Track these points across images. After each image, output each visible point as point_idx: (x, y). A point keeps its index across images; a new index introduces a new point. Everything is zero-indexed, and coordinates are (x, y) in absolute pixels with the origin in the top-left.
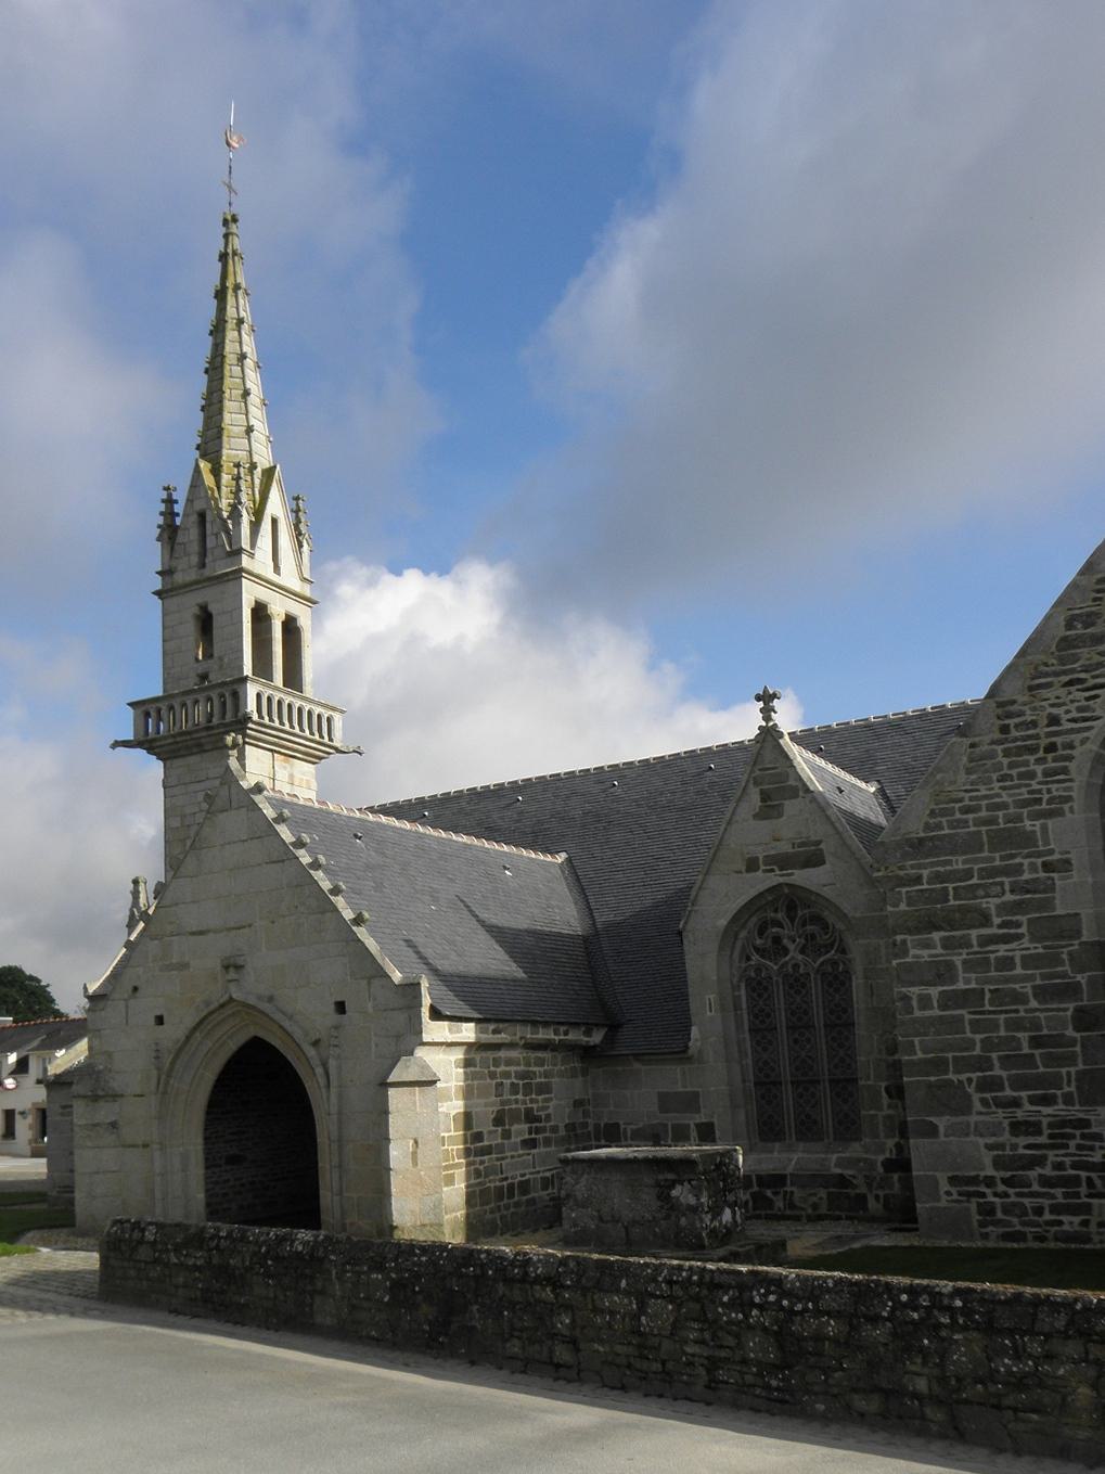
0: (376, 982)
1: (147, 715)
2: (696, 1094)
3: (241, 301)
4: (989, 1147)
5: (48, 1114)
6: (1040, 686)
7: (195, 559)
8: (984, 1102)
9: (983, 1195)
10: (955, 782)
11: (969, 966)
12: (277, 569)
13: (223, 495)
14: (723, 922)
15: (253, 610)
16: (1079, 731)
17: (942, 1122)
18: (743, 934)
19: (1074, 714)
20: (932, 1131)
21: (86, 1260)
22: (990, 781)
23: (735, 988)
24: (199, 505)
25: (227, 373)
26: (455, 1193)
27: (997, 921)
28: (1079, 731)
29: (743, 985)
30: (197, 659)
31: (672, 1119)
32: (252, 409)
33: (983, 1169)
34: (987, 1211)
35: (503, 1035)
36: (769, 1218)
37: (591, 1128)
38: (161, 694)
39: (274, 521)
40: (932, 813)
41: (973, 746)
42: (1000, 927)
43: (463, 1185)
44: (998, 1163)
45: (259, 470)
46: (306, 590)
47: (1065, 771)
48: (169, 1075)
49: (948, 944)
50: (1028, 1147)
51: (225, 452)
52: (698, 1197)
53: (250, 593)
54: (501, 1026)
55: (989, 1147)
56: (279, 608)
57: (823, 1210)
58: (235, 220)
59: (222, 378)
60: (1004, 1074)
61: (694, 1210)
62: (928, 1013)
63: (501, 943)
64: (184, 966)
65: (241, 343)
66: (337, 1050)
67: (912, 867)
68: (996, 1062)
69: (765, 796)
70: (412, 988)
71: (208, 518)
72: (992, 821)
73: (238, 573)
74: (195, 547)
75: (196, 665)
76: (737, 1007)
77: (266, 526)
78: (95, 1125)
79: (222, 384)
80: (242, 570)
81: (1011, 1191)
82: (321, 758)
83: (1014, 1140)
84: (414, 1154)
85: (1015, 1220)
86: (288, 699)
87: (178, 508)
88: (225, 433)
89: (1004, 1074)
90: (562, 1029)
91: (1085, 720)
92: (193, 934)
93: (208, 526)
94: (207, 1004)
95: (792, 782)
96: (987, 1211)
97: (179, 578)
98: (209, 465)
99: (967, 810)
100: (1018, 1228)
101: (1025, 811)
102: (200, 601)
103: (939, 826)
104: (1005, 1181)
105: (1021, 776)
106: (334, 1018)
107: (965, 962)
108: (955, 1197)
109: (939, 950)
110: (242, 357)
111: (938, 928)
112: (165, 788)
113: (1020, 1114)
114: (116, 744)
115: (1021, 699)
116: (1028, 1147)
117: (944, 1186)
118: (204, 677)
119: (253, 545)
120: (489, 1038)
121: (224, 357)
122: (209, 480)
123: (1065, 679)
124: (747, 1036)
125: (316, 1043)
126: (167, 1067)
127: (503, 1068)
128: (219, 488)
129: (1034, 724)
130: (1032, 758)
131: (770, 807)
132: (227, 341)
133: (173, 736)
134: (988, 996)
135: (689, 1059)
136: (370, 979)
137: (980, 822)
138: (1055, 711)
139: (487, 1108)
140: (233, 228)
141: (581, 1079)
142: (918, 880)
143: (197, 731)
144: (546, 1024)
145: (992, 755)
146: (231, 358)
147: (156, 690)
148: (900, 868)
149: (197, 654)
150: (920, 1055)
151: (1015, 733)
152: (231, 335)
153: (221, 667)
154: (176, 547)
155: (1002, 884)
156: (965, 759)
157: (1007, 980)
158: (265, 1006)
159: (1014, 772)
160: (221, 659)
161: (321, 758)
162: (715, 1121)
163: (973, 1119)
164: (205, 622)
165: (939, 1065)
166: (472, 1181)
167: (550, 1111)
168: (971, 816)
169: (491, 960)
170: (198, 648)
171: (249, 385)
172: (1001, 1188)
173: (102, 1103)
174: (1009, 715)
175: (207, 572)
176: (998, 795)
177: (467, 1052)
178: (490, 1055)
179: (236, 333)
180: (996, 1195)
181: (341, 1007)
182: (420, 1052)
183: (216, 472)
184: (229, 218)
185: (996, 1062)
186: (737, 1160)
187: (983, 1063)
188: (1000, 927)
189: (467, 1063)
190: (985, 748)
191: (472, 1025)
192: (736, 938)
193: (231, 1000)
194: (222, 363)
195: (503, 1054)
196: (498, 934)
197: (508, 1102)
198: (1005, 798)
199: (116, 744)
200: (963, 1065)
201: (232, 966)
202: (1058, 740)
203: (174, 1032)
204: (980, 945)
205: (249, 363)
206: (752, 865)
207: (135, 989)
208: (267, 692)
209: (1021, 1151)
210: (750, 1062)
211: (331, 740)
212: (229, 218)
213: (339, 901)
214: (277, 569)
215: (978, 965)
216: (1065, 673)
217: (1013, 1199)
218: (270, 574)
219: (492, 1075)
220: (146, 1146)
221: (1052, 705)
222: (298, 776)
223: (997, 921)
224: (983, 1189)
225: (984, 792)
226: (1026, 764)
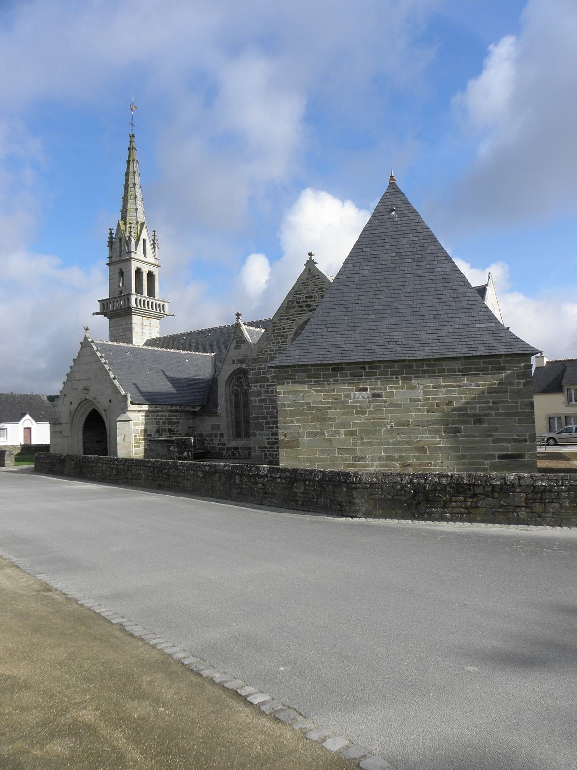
0: (119, 394)
1: (104, 304)
2: (219, 425)
3: (135, 164)
4: (267, 439)
5: (26, 427)
6: (281, 319)
7: (118, 253)
8: (266, 427)
9: (265, 451)
10: (263, 344)
11: (265, 392)
12: (145, 256)
13: (127, 232)
14: (226, 378)
15: (136, 271)
16: (289, 331)
17: (258, 432)
18: (233, 381)
19: (288, 327)
20: (255, 435)
21: (32, 466)
22: (270, 344)
23: (230, 396)
24: (119, 236)
25: (129, 190)
26: (142, 448)
27: (271, 381)
28: (289, 331)
29: (233, 395)
30: (119, 286)
31: (215, 432)
32: (138, 202)
33: (265, 444)
34: (266, 455)
35: (159, 408)
36: (235, 459)
37: (196, 434)
38: (108, 297)
39: (144, 240)
40: (258, 352)
41: (267, 334)
42: (271, 382)
43: (143, 448)
44: (269, 443)
45: (140, 223)
46: (157, 262)
47: (286, 342)
48: (73, 418)
49: (261, 387)
50: (275, 439)
51: (128, 217)
52: (174, 449)
53: (134, 265)
54: (158, 406)
55: (267, 439)
56: (145, 270)
57: (247, 457)
58: (133, 136)
59: (128, 192)
60: (271, 420)
61: (174, 452)
62: (256, 404)
63: (171, 382)
64: (76, 389)
65: (134, 179)
66: (110, 412)
67: (254, 366)
68: (269, 417)
69: (237, 343)
70: (126, 396)
71: (122, 240)
72: (270, 354)
73: (130, 259)
74: (118, 250)
75: (118, 288)
76: (231, 401)
77: (141, 242)
78: (56, 432)
79: (128, 194)
80: (131, 258)
81: (271, 450)
82: (161, 318)
83: (272, 437)
84: (124, 439)
85: (271, 458)
86: (151, 301)
87: (114, 236)
88: (128, 211)
89: (271, 420)
90: (182, 407)
91: (290, 329)
92: (78, 380)
93: (122, 242)
94: (81, 399)
95: (243, 339)
96: (266, 455)
97: (114, 259)
98: (123, 222)
99: (266, 351)
100: (272, 459)
101: (277, 352)
102: (120, 267)
103: (259, 355)
104: (269, 448)
105: (277, 343)
106: (109, 404)
107: (264, 391)
108: (260, 452)
109: (259, 388)
110: (135, 184)
111: (259, 382)
112: (110, 327)
113: (273, 431)
114: (94, 314)
115: (278, 322)
116: (275, 439)
117: (257, 449)
118: (121, 292)
119: (136, 249)
120: (151, 409)
121: (128, 185)
122: (122, 227)
123: (287, 317)
124: (234, 409)
125: (105, 410)
126: (73, 415)
127: (159, 417)
128: (126, 230)
129: (280, 329)
130: (279, 338)
131: (238, 347)
132: (130, 179)
133: (111, 311)
134: (268, 400)
135: (218, 415)
136: (117, 393)
137: (268, 355)
138: (284, 326)
139: (153, 428)
140: (133, 139)
141: (192, 420)
142: (255, 369)
143: (118, 310)
144: (176, 405)
145: (271, 337)
146: (131, 185)
147: (107, 296)
148: (252, 366)
149: (119, 285)
150: (254, 415)
151: (276, 331)
152: (131, 177)
153: (126, 289)
154: (113, 249)
155: (272, 371)
156: (265, 338)
157: (272, 396)
158: (93, 400)
159: (275, 342)
160: (126, 287)
161: (161, 318)
162: (224, 432)
163: (264, 432)
164: (121, 273)
165: (257, 418)
166: (147, 447)
167: (179, 429)
168: (266, 353)
169: (166, 387)
170: (120, 282)
171: (137, 194)
172: (269, 449)
173: (57, 426)
174: (275, 326)
175: (122, 258)
176: (272, 348)
177: (146, 413)
178: (155, 414)
179: (133, 176)
180: (268, 451)
181: (110, 401)
182: (128, 413)
183: (125, 224)
184: (131, 135)
185: (269, 417)
186: (191, 441)
187: (266, 418)
188: (271, 382)
189: (146, 416)
190: (270, 335)
191: (147, 406)
192: (231, 382)
193: (86, 399)
194: (128, 186)
195: (160, 413)
196: (172, 380)
197: (162, 426)
198: (273, 349)
199: (94, 314)
200: (263, 418)
201: (86, 389)
202: (284, 333)
203: (74, 406)
204: (267, 387)
205: (137, 186)
206: (233, 362)
207: (65, 395)
208: (143, 299)
209: (273, 440)
210: (234, 416)
211: (164, 312)
212: (131, 135)
213: (110, 373)
214: (145, 256)
215: (266, 392)
216: (287, 316)
217: (271, 452)
218: (143, 259)
219: (155, 419)
220: (68, 437)
221: (284, 324)
222: (152, 324)
223: (271, 381)
224: (265, 450)
225: (269, 347)
226: (278, 339)
